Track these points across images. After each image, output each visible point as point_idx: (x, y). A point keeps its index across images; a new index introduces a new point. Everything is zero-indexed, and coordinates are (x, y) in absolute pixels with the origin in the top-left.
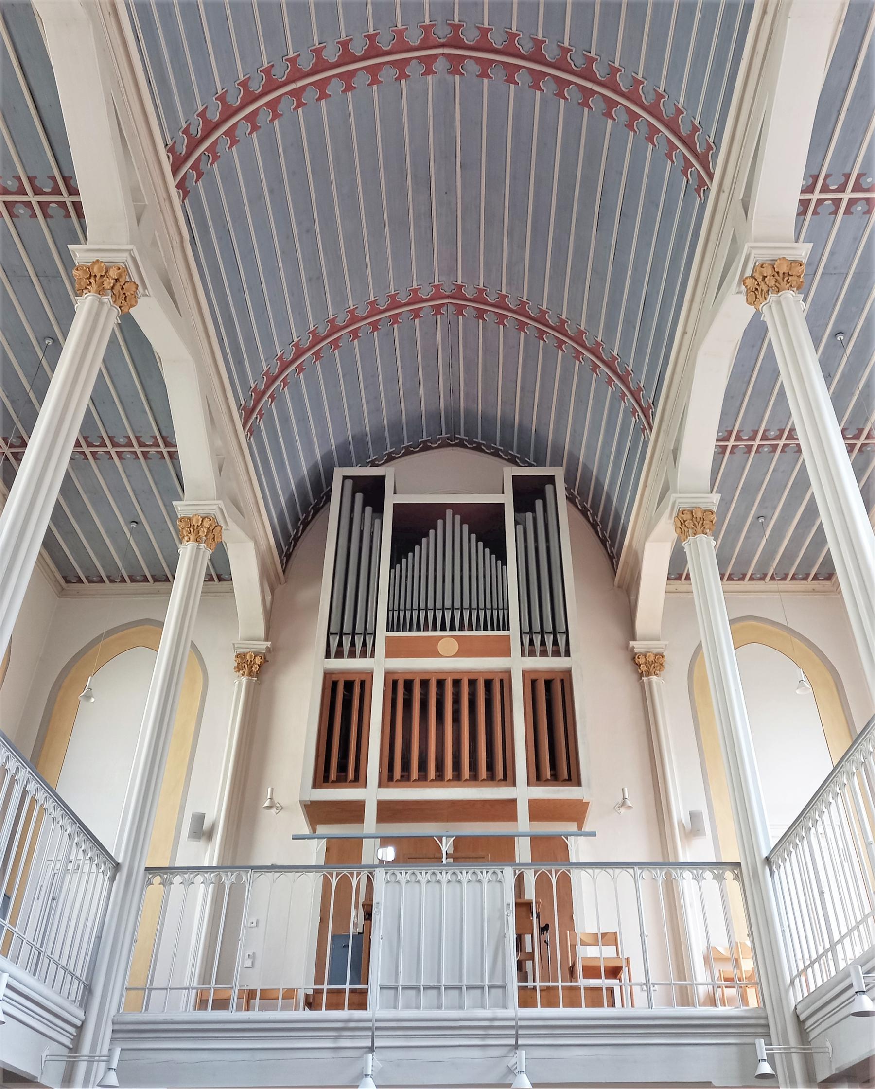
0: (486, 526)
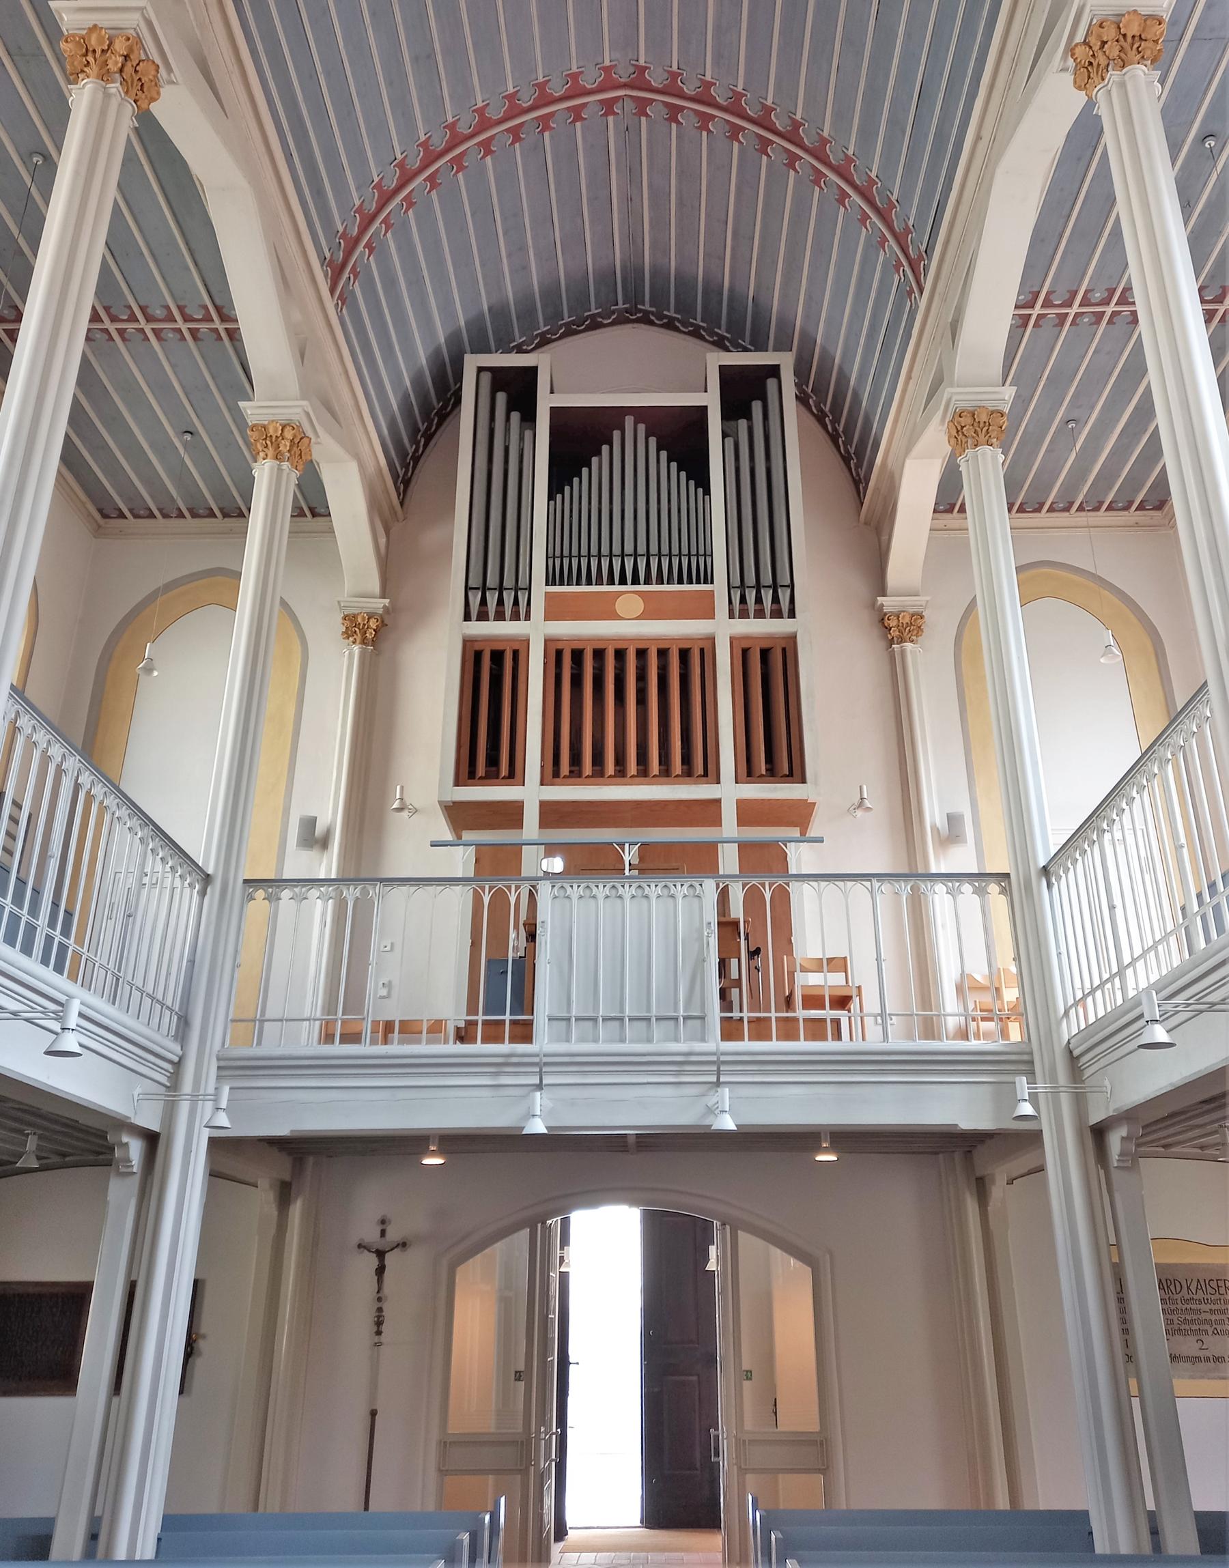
0: (681, 438)
